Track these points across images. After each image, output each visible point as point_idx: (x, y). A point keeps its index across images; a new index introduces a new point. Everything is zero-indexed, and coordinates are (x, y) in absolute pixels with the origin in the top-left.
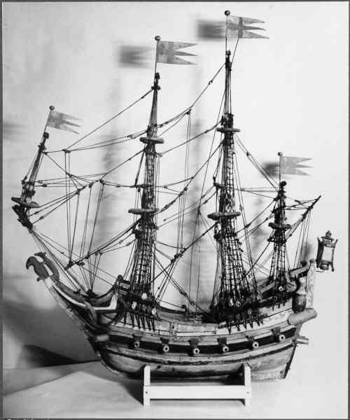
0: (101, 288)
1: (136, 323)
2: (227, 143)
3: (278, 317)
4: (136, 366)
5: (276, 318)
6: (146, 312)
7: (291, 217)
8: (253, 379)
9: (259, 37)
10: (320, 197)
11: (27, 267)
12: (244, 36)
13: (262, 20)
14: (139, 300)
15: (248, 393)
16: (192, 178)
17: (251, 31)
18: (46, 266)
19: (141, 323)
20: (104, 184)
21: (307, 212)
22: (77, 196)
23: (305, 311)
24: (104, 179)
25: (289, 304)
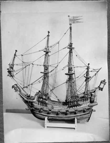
0: (33, 94)
1: (42, 105)
2: (71, 52)
3: (85, 105)
5: (85, 105)
6: (45, 102)
7: (91, 74)
8: (78, 122)
9: (80, 22)
10: (101, 68)
11: (12, 88)
12: (75, 22)
14: (43, 99)
15: (76, 126)
16: (60, 62)
17: (77, 21)
18: (17, 88)
20: (33, 65)
21: (97, 73)
22: (25, 68)
23: (94, 103)
24: (33, 63)
25: (89, 101)
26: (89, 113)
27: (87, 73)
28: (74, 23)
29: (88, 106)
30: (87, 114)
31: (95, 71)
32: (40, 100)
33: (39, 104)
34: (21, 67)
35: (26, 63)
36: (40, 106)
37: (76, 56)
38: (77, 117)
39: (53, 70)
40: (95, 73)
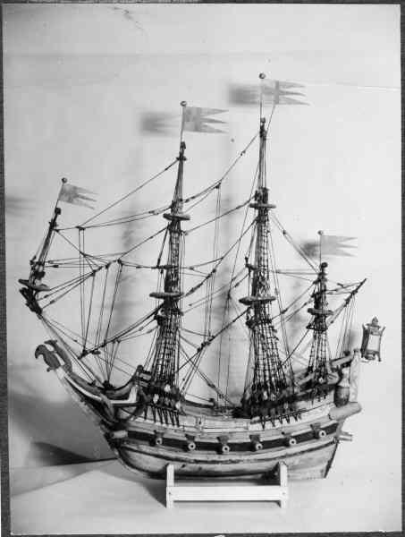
0: (119, 379)
1: (158, 418)
2: (261, 220)
3: (317, 412)
5: (317, 413)
6: (170, 406)
7: (333, 302)
8: (290, 479)
14: (162, 393)
18: (57, 355)
21: (351, 297)
22: (91, 278)
24: (122, 259)
25: (331, 397)
26: (332, 443)
27: (318, 298)
30: (327, 445)
31: (343, 290)
32: (152, 401)
33: (155, 420)
34: (76, 273)
35: (94, 257)
36: (153, 422)
38: (288, 461)
39: (199, 286)
40: (346, 298)
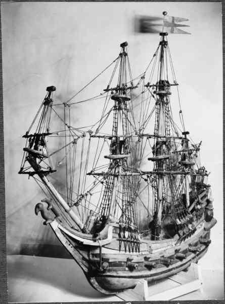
4: (144, 246)
9: (186, 33)
10: (190, 34)
13: (186, 18)
14: (129, 230)
19: (134, 249)
28: (172, 32)
29: (205, 228)
32: (124, 237)
37: (181, 112)
